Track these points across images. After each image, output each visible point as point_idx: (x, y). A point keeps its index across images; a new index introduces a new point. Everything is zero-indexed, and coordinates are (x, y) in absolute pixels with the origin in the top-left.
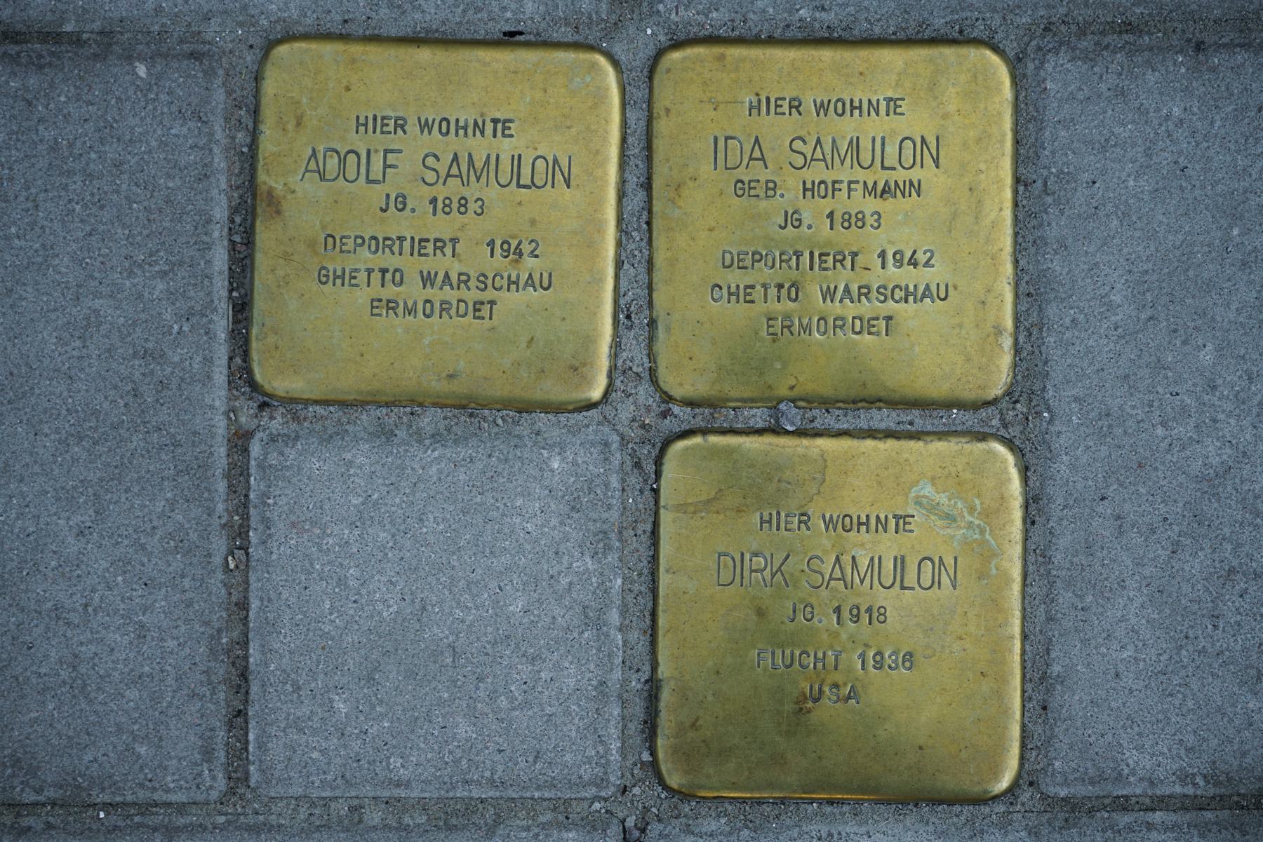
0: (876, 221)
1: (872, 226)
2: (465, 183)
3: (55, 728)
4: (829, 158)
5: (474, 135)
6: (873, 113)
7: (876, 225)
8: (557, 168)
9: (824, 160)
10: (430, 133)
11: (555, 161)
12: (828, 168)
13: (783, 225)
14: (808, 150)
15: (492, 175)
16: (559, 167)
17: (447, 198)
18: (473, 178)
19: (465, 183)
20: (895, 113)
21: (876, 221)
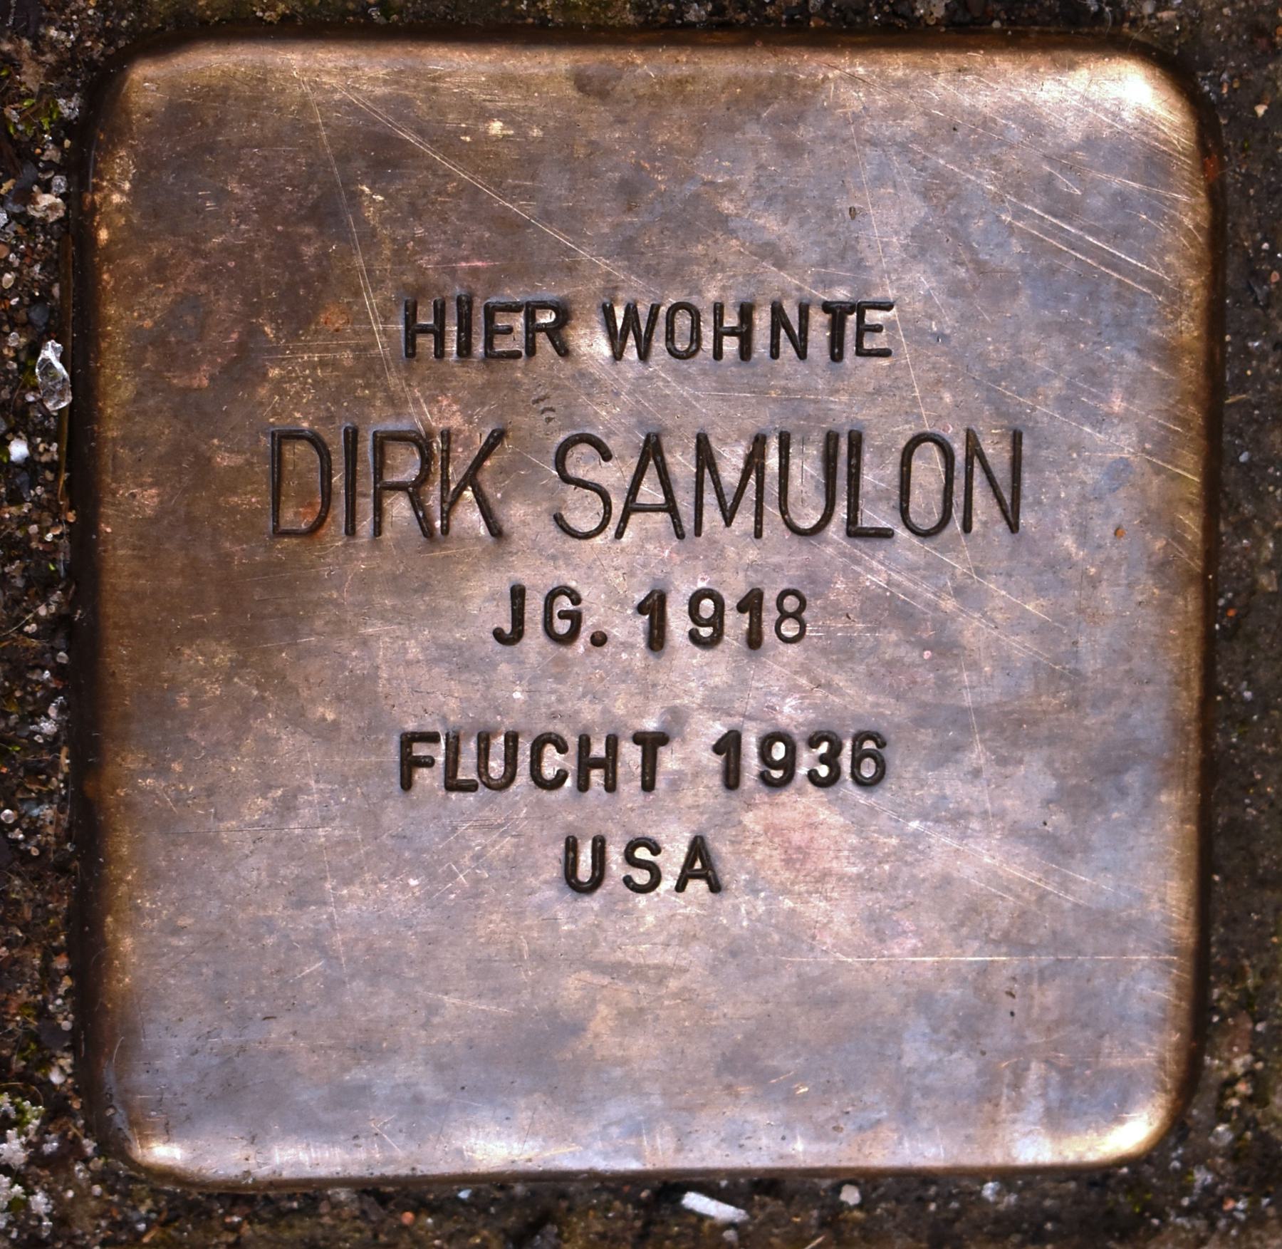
0: (823, 759)
1: (813, 777)
2: (688, 525)
3: (238, 1055)
4: (685, 504)
5: (775, 353)
6: (787, 349)
7: (823, 771)
8: (1007, 497)
9: (670, 507)
10: (644, 355)
11: (974, 450)
12: (680, 535)
13: (507, 628)
14: (614, 476)
15: (771, 510)
16: (1000, 501)
17: (794, 593)
18: (712, 515)
19: (688, 525)
20: (860, 352)
21: (823, 759)
